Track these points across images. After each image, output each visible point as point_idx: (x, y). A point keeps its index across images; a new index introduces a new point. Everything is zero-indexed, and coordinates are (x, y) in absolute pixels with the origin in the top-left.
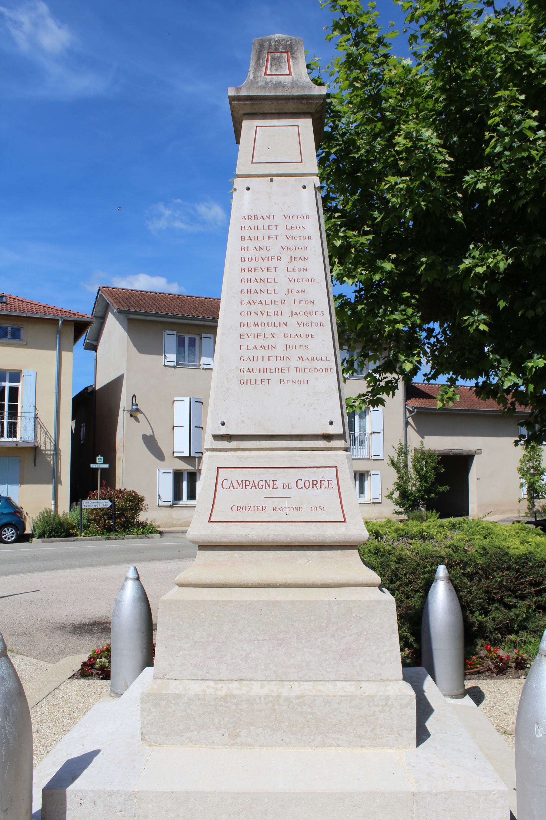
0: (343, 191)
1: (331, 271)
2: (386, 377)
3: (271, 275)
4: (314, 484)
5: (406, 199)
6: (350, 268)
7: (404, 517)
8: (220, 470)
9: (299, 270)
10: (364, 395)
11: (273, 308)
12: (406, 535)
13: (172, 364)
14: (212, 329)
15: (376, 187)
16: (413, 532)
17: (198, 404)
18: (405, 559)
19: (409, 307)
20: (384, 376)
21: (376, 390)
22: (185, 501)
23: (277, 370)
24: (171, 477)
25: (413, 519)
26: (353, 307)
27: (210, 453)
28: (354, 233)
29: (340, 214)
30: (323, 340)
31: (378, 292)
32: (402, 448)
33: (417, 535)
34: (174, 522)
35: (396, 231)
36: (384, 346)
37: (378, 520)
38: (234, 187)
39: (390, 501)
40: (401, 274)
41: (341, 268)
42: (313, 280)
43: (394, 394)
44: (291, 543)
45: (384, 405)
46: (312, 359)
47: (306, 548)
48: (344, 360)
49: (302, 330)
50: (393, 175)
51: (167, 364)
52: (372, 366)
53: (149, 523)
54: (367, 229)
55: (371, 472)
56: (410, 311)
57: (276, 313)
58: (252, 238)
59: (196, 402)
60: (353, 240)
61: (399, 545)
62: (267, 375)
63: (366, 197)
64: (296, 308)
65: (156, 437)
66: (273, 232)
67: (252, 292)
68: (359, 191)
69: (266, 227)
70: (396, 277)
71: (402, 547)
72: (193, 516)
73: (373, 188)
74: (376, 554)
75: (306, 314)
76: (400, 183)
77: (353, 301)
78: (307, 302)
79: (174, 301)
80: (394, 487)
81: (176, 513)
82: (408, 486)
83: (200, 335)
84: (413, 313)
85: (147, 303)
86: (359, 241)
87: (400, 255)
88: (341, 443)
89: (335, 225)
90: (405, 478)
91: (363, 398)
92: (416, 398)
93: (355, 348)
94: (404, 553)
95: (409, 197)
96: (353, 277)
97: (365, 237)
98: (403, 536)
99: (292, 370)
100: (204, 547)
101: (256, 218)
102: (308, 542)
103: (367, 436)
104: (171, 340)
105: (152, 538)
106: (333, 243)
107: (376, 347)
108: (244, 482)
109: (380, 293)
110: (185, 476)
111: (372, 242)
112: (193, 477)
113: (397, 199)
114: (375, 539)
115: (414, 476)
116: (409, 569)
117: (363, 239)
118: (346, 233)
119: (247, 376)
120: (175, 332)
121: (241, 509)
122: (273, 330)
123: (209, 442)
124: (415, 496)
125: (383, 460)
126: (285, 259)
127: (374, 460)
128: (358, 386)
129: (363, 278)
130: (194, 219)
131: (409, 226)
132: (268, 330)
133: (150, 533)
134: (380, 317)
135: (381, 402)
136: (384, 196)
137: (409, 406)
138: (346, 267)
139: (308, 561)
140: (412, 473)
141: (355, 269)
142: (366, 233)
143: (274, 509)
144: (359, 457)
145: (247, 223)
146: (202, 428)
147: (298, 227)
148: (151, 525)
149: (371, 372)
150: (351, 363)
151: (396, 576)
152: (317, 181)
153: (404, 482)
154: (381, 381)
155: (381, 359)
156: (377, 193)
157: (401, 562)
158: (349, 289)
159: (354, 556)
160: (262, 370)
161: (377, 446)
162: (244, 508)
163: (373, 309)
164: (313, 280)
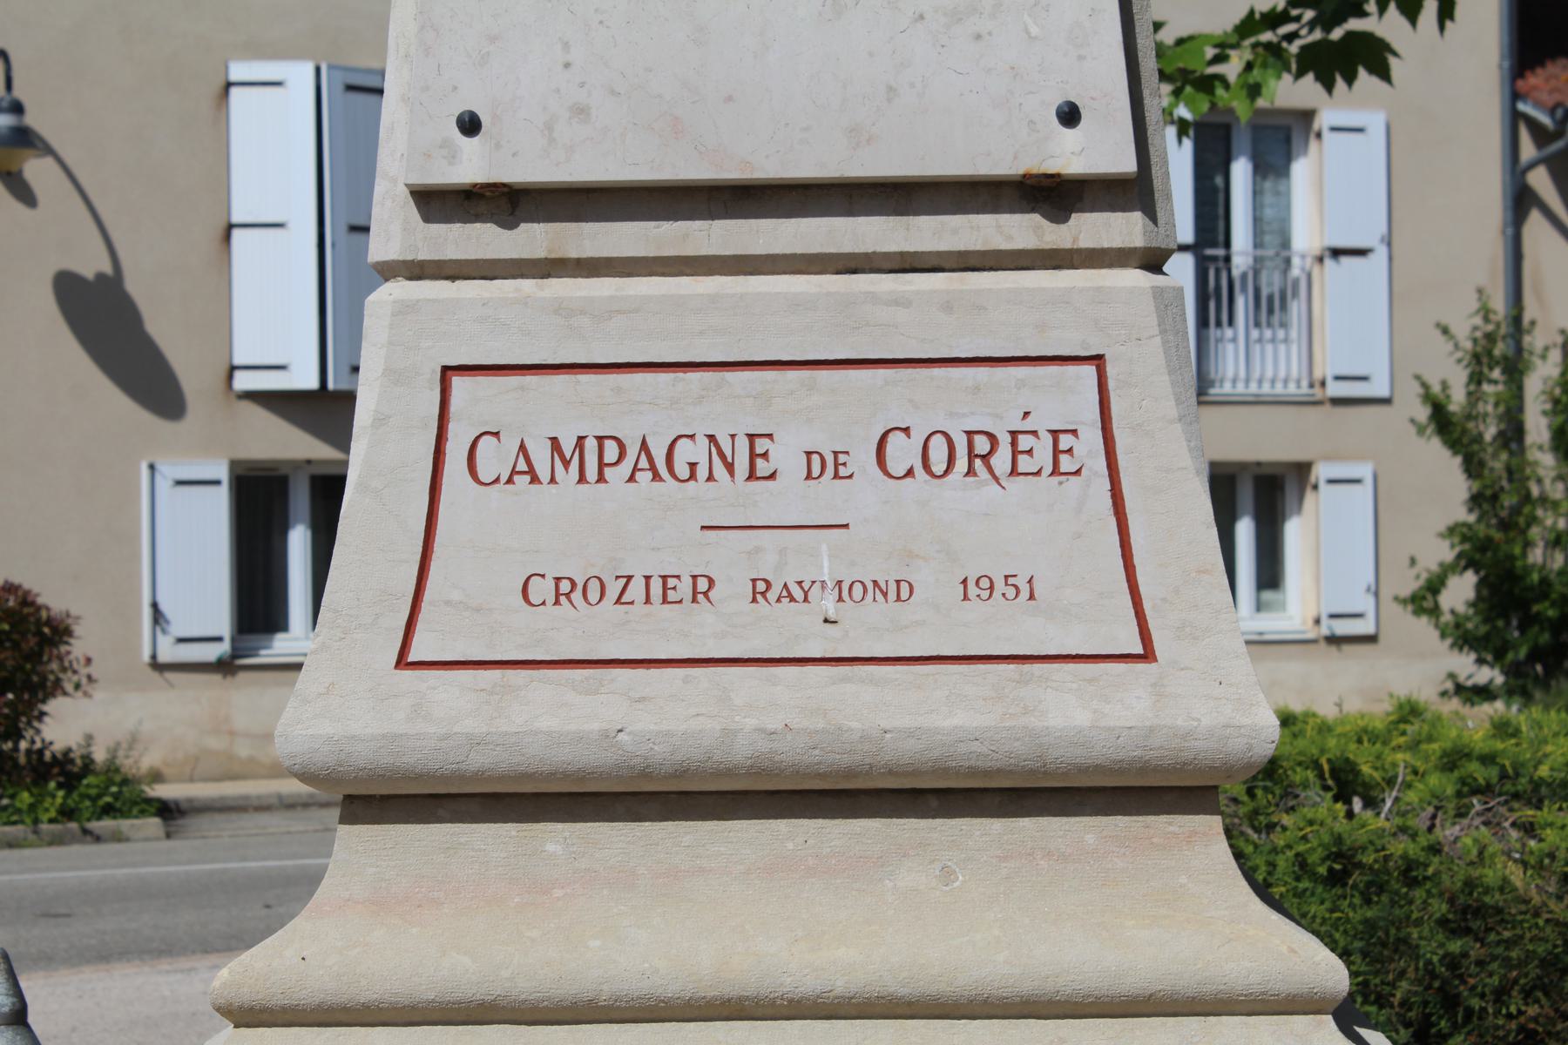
4: (979, 453)
8: (457, 382)
12: (1508, 787)
16: (1544, 771)
18: (1499, 911)
24: (216, 508)
27: (397, 290)
32: (1490, 338)
34: (243, 750)
44: (850, 773)
45: (1383, 73)
53: (100, 756)
55: (1321, 472)
59: (351, 88)
65: (132, 286)
74: (1335, 879)
80: (1446, 552)
82: (1528, 544)
90: (1508, 501)
91: (1267, 36)
94: (1490, 876)
98: (1485, 790)
100: (382, 800)
102: (945, 771)
103: (1295, 271)
105: (118, 838)
108: (591, 445)
110: (300, 499)
116: (1522, 964)
121: (577, 596)
123: (396, 230)
125: (1386, 401)
133: (108, 811)
135: (1372, 56)
137: (1538, 104)
139: (947, 874)
143: (760, 590)
144: (1253, 388)
148: (112, 769)
151: (1451, 1002)
153: (1504, 526)
157: (1476, 924)
159: (1200, 847)
161: (1353, 330)
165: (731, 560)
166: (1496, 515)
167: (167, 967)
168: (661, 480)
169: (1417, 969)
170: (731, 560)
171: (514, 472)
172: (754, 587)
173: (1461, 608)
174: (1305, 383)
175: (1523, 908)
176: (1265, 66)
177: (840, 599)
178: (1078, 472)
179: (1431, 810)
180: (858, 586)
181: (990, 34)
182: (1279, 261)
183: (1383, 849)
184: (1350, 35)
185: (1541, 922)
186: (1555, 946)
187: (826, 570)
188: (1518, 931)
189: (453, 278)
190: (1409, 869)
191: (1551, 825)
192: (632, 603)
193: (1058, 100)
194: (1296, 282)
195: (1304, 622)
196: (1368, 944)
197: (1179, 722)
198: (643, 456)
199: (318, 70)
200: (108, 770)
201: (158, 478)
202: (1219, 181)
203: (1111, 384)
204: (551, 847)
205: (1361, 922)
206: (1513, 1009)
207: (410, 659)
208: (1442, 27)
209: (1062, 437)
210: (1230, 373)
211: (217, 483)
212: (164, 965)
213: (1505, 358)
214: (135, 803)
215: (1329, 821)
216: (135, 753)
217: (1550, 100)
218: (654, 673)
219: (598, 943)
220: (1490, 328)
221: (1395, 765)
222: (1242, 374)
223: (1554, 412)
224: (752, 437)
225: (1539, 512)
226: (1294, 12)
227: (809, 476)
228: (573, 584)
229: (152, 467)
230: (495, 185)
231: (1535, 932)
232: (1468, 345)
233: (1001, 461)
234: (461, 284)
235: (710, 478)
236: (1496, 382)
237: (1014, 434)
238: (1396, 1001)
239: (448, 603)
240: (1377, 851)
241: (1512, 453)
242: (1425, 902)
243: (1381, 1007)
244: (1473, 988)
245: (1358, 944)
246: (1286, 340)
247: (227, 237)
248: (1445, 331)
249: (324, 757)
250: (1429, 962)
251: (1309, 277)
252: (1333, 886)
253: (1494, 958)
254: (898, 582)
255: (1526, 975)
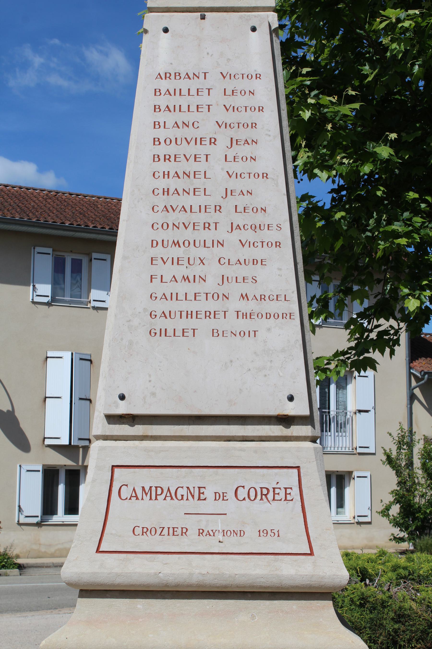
0: (315, 33)
1: (294, 159)
2: (379, 326)
3: (200, 166)
4: (264, 494)
5: (413, 46)
6: (325, 154)
7: (405, 546)
9: (244, 159)
10: (343, 353)
11: (201, 218)
13: (46, 300)
14: (109, 247)
15: (367, 26)
16: (421, 572)
17: (85, 363)
18: (409, 616)
19: (416, 215)
20: (375, 323)
21: (362, 346)
22: (61, 516)
23: (208, 314)
24: (38, 478)
25: (422, 551)
26: (327, 215)
28: (331, 98)
29: (309, 69)
30: (280, 269)
31: (367, 192)
33: (427, 577)
34: (43, 549)
35: (397, 97)
36: (376, 277)
37: (366, 551)
38: (145, 26)
39: (385, 520)
40: (404, 165)
41: (310, 154)
42: (265, 176)
43: (392, 353)
44: (226, 587)
45: (375, 369)
46: (262, 298)
47: (250, 595)
48: (313, 298)
49: (248, 253)
50: (395, 7)
51: (37, 299)
52: (357, 307)
54: (352, 93)
55: (355, 474)
56: (418, 220)
57: (207, 225)
58: (172, 109)
59: (81, 359)
60: (330, 110)
61: (399, 592)
62: (192, 323)
63: (351, 41)
64: (239, 219)
65: (17, 414)
66: (204, 100)
67: (171, 192)
68: (341, 32)
69: (193, 92)
70: (397, 168)
71: (403, 596)
72: (71, 541)
73: (362, 28)
74: (361, 606)
75: (254, 228)
76: (404, 19)
77: (328, 206)
78: (255, 210)
79: (49, 201)
81: (46, 535)
82: (414, 496)
83: (89, 254)
84: (423, 223)
85: (6, 204)
86: (339, 111)
87: (403, 134)
88: (305, 430)
89: (302, 86)
90: (409, 484)
91: (342, 358)
92: (426, 358)
93: (330, 280)
94: (407, 606)
95: (418, 42)
96: (329, 168)
97: (348, 106)
98: (405, 578)
99: (231, 315)
100: (90, 592)
101: (178, 77)
102: (253, 587)
103: (348, 416)
104: (43, 262)
106: (299, 115)
107: (363, 278)
108: (153, 489)
109: (371, 194)
110: (62, 476)
111: (359, 114)
112: (74, 478)
113: (399, 45)
114: (361, 581)
115: (423, 481)
116: (416, 632)
117: (346, 109)
118: (319, 99)
119: (161, 323)
120: (50, 250)
121: (148, 533)
122: (202, 252)
123: (99, 426)
124: (425, 512)
125: (374, 454)
126: (223, 141)
127: (360, 454)
128: (334, 339)
129: (344, 170)
130: (81, 71)
131: (418, 87)
132: (195, 252)
134: (370, 231)
135: (371, 364)
136: (381, 40)
137: (416, 370)
138: (318, 153)
139: (253, 617)
140: (420, 477)
141: (332, 156)
142: (350, 100)
143: (201, 532)
144: (336, 450)
145: (164, 85)
146: (90, 401)
147: (243, 93)
149: (355, 316)
150: (324, 303)
152: (273, 18)
153: (408, 491)
154: (371, 331)
155: (371, 297)
156: (368, 36)
157: (402, 620)
158: (322, 187)
160: (184, 314)
161: (364, 433)
162: (153, 530)
163: (360, 218)
164: (265, 176)
165: (193, 524)
166: (405, 488)
167: (19, 615)
168: (173, 500)
169: (385, 632)
170: (193, 524)
171: (131, 496)
172: (199, 531)
173: (395, 515)
174: (351, 449)
175: (416, 615)
176: (341, 366)
177: (224, 535)
178: (292, 500)
179: (389, 583)
180: (229, 532)
181: (269, 375)
182: (343, 413)
183: (376, 597)
184: (364, 357)
185: (421, 620)
186: (425, 627)
187: (220, 527)
188: (415, 622)
189: (116, 440)
190: (383, 603)
191: (424, 590)
192: (164, 535)
193: (287, 394)
194: (348, 420)
195: (350, 518)
196: (371, 625)
197: (320, 574)
198: (168, 492)
199: (72, 354)
200: (4, 555)
201: (22, 468)
202: (327, 390)
203: (302, 475)
204: (139, 606)
205: (369, 619)
206: (413, 645)
207: (100, 550)
208: (391, 357)
209: (288, 490)
210: (329, 446)
211: (39, 471)
212: (18, 615)
213: (407, 442)
214: (11, 565)
215: (360, 588)
216: (12, 550)
217: (420, 369)
218: (170, 556)
219: (152, 635)
220: (403, 434)
221: (378, 569)
222: (333, 446)
223: (422, 458)
224: (199, 488)
225: (418, 487)
226: (350, 351)
227: (215, 500)
228: (147, 529)
229: (20, 466)
230: (129, 414)
231: (419, 622)
232: (397, 439)
233: (270, 496)
234: (118, 442)
235: (187, 499)
236: (405, 449)
237: (274, 489)
238: (379, 642)
239: (111, 534)
240: (374, 597)
241: (410, 470)
242: (388, 613)
243: (375, 644)
244: (401, 639)
245: (368, 625)
246: (345, 436)
247: (45, 401)
248: (390, 435)
249: (74, 579)
250: (389, 631)
251: (352, 418)
252: (361, 608)
253: (408, 630)
254: (240, 531)
255: (417, 635)
